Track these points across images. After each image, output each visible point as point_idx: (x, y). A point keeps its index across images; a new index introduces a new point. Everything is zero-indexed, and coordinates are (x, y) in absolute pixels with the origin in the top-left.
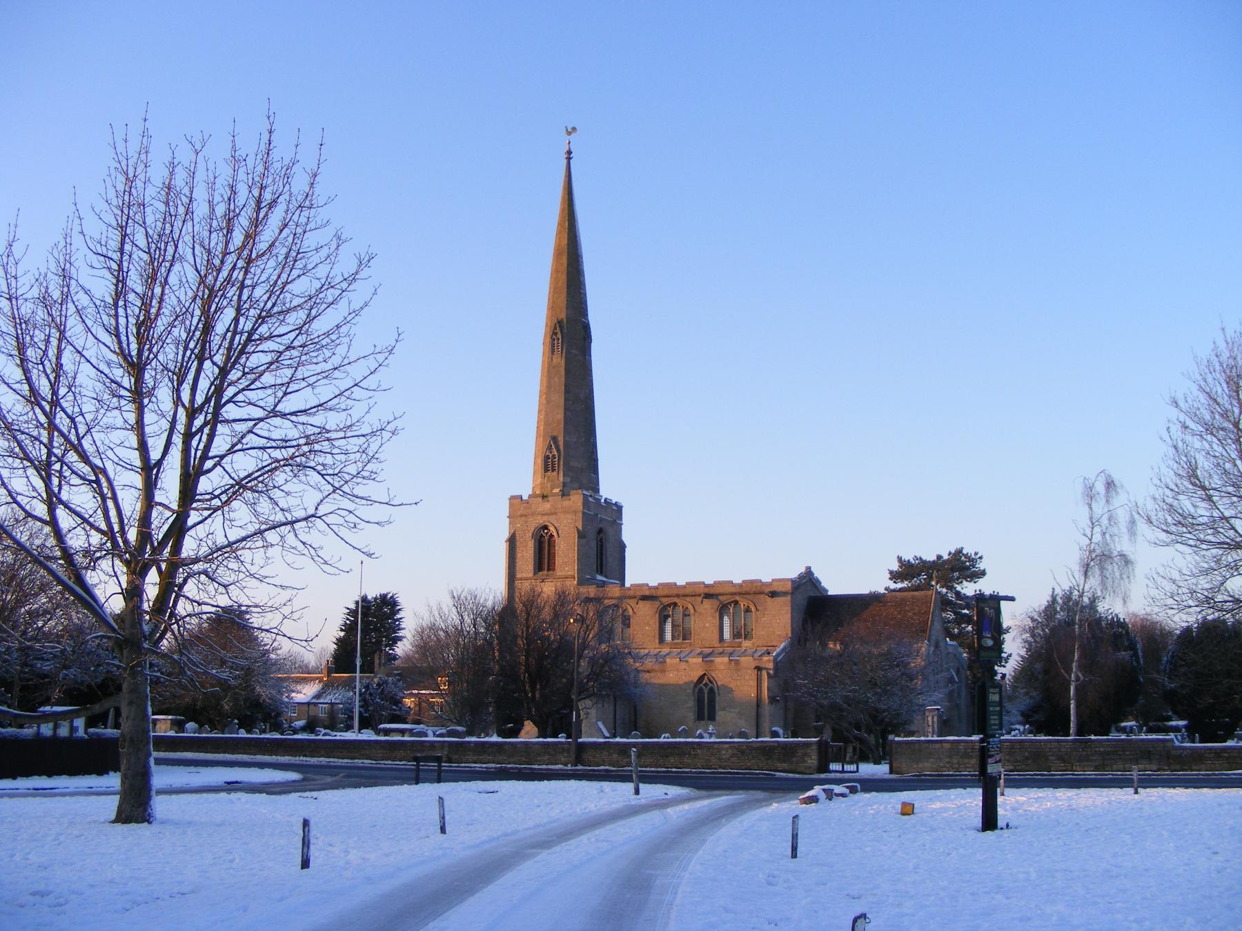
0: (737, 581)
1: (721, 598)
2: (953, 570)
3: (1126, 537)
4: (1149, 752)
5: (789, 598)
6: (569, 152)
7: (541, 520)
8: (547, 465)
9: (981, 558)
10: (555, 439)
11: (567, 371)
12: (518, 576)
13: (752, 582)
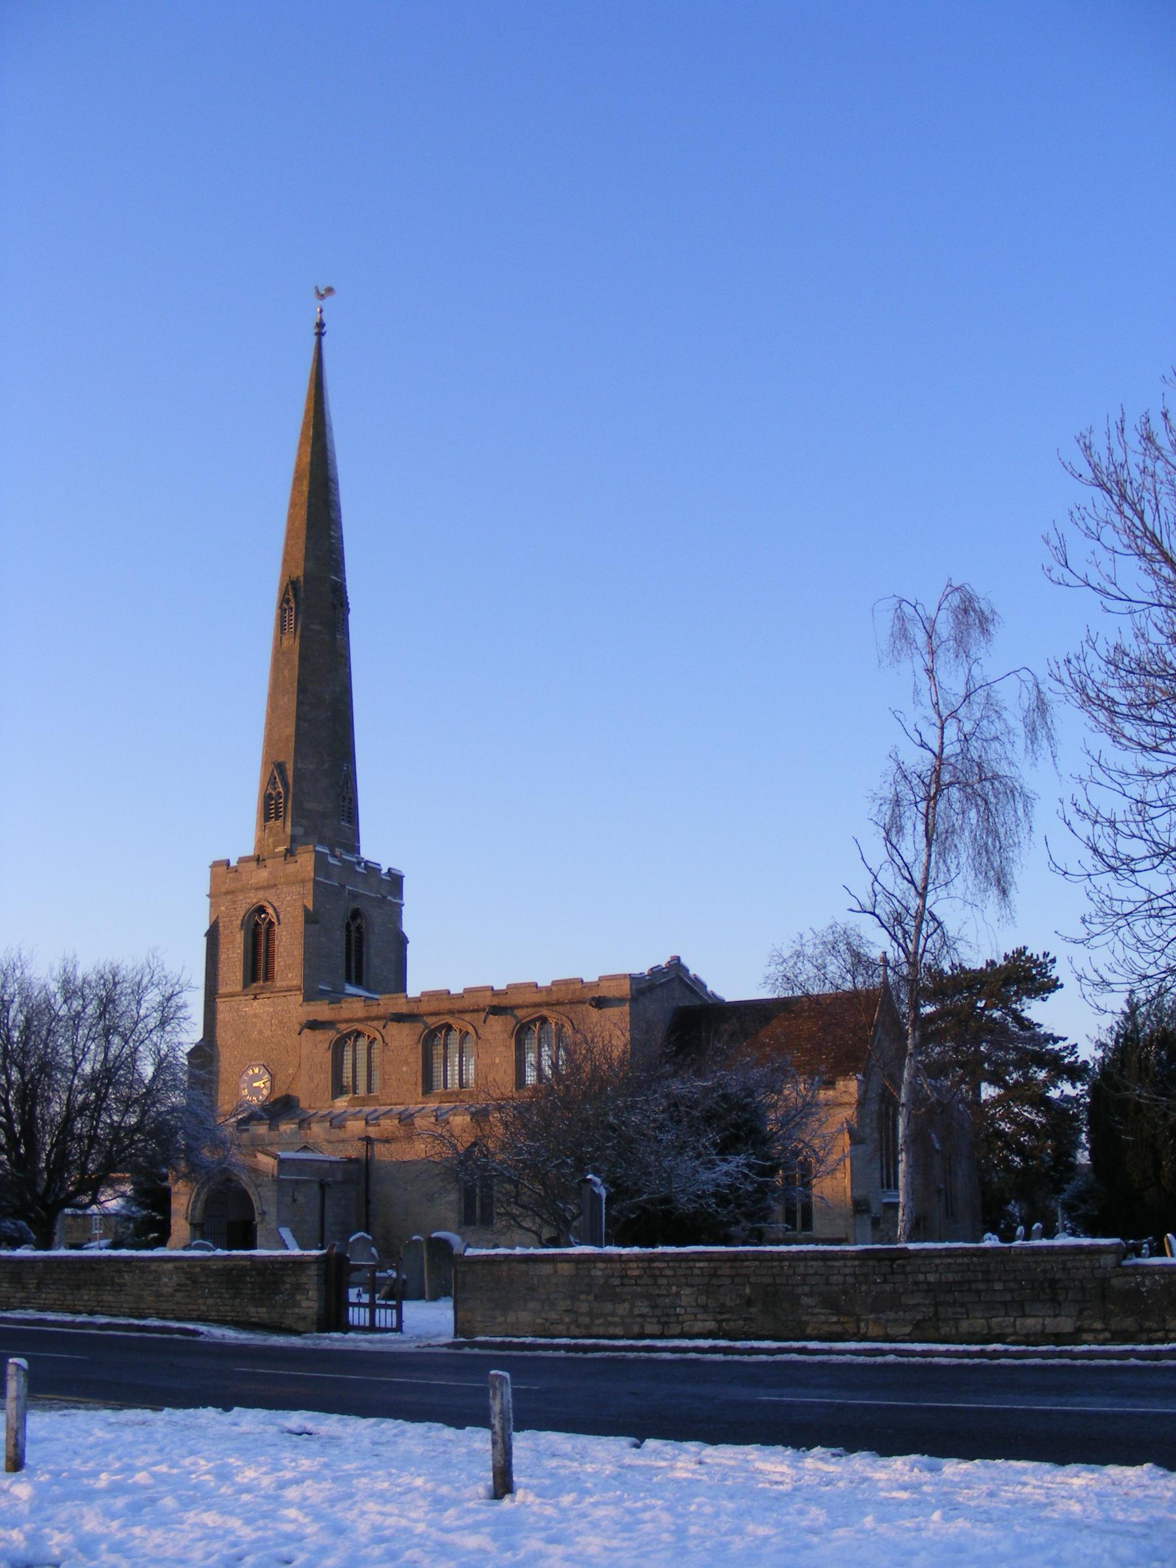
0: (544, 982)
1: (520, 1013)
2: (1007, 982)
3: (1021, 743)
4: (1053, 1283)
5: (626, 1008)
6: (321, 325)
7: (254, 898)
8: (270, 809)
9: (1053, 961)
10: (280, 767)
11: (303, 658)
12: (222, 990)
13: (567, 983)
